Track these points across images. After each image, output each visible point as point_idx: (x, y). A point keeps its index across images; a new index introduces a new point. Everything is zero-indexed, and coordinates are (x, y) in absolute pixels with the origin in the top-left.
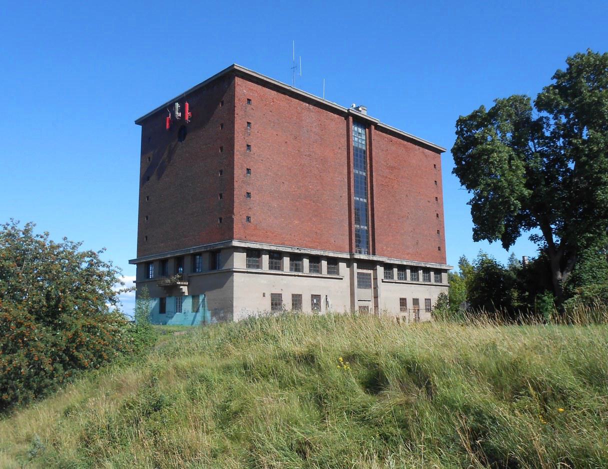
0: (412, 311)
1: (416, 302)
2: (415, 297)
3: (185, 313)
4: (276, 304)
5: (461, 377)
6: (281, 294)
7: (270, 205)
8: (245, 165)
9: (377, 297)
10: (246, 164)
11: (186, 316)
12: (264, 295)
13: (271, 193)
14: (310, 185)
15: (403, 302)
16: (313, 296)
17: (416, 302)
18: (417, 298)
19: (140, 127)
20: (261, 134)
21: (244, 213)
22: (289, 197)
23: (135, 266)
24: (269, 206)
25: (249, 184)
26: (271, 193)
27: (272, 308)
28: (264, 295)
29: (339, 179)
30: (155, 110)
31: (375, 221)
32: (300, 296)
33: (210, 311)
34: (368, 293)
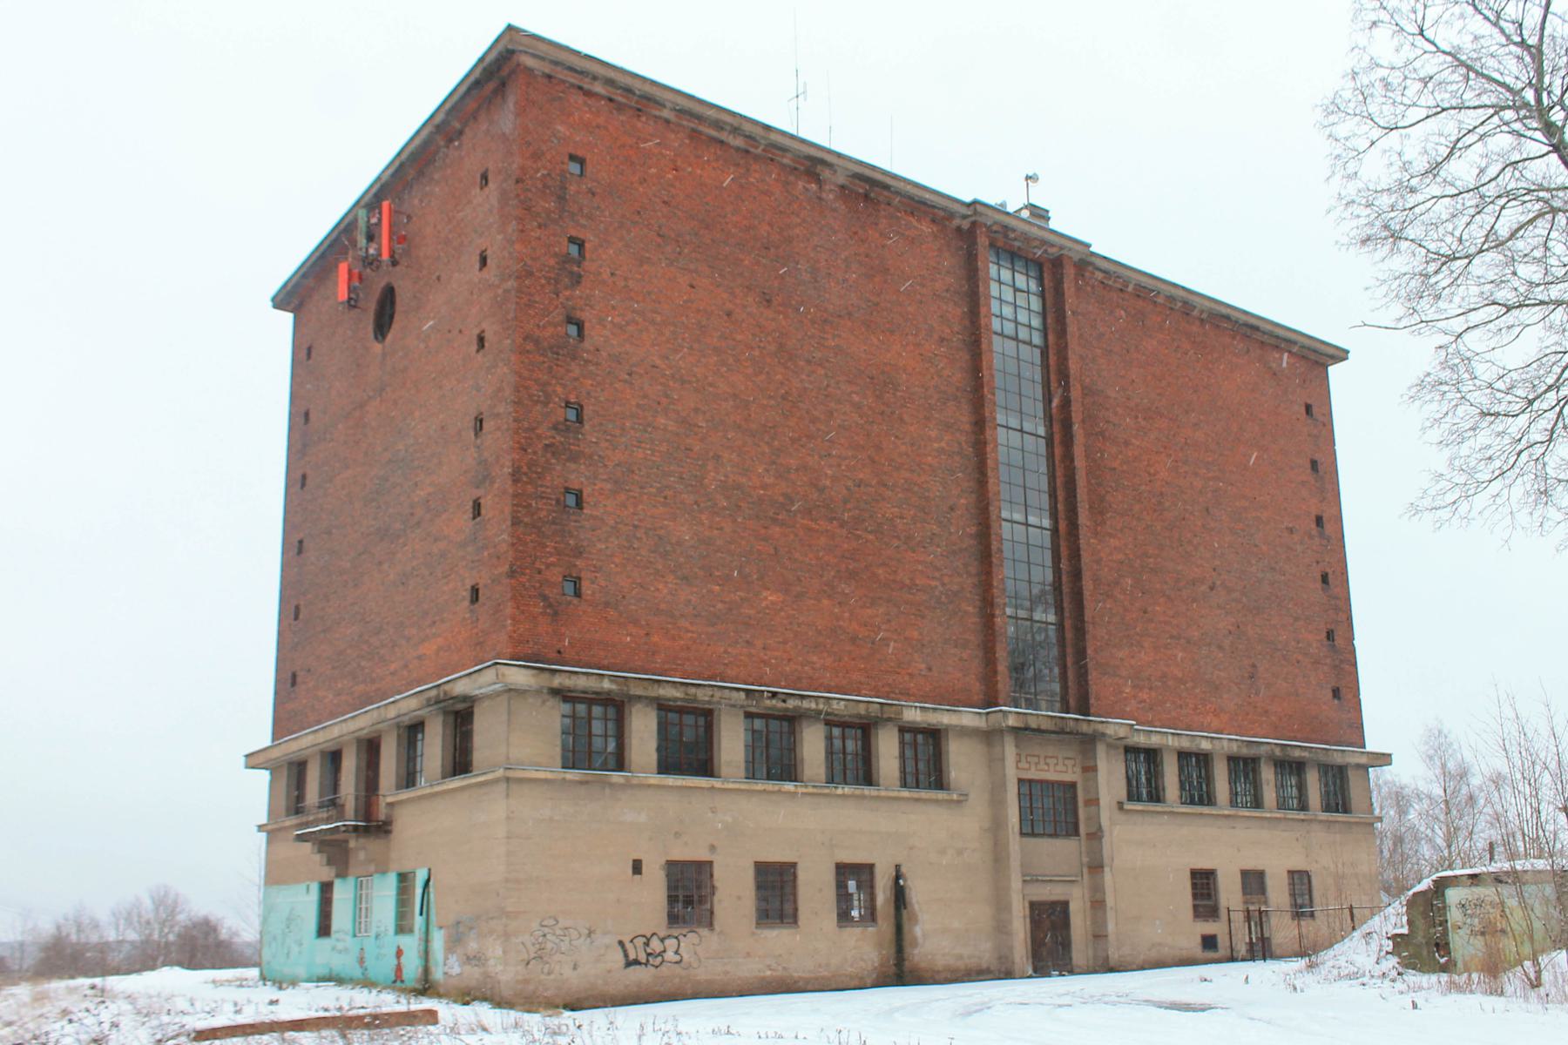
0: (1238, 918)
1: (1253, 881)
2: (1251, 864)
3: (377, 936)
4: (689, 902)
5: (1466, 43)
6: (711, 863)
7: (662, 532)
8: (559, 389)
9: (1102, 867)
10: (564, 386)
11: (378, 947)
12: (637, 867)
13: (669, 493)
14: (830, 466)
15: (1203, 882)
16: (844, 871)
17: (1253, 881)
18: (1260, 868)
19: (287, 318)
20: (626, 279)
21: (552, 564)
22: (739, 507)
23: (265, 776)
24: (660, 538)
25: (574, 458)
26: (669, 493)
27: (673, 919)
28: (637, 867)
29: (943, 444)
30: (317, 249)
31: (1087, 594)
32: (703, 869)
33: (442, 932)
34: (1059, 853)
